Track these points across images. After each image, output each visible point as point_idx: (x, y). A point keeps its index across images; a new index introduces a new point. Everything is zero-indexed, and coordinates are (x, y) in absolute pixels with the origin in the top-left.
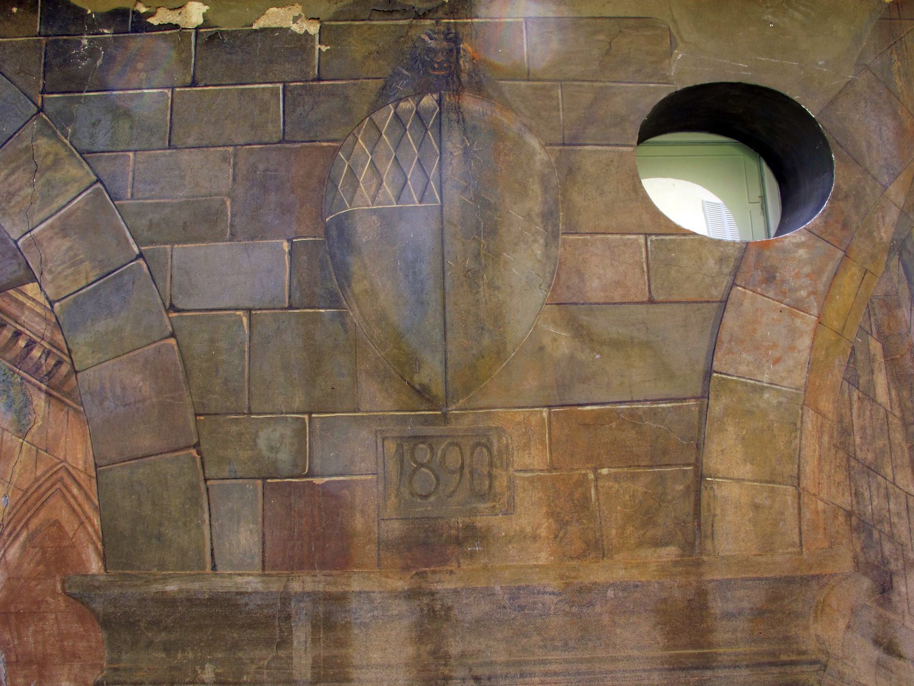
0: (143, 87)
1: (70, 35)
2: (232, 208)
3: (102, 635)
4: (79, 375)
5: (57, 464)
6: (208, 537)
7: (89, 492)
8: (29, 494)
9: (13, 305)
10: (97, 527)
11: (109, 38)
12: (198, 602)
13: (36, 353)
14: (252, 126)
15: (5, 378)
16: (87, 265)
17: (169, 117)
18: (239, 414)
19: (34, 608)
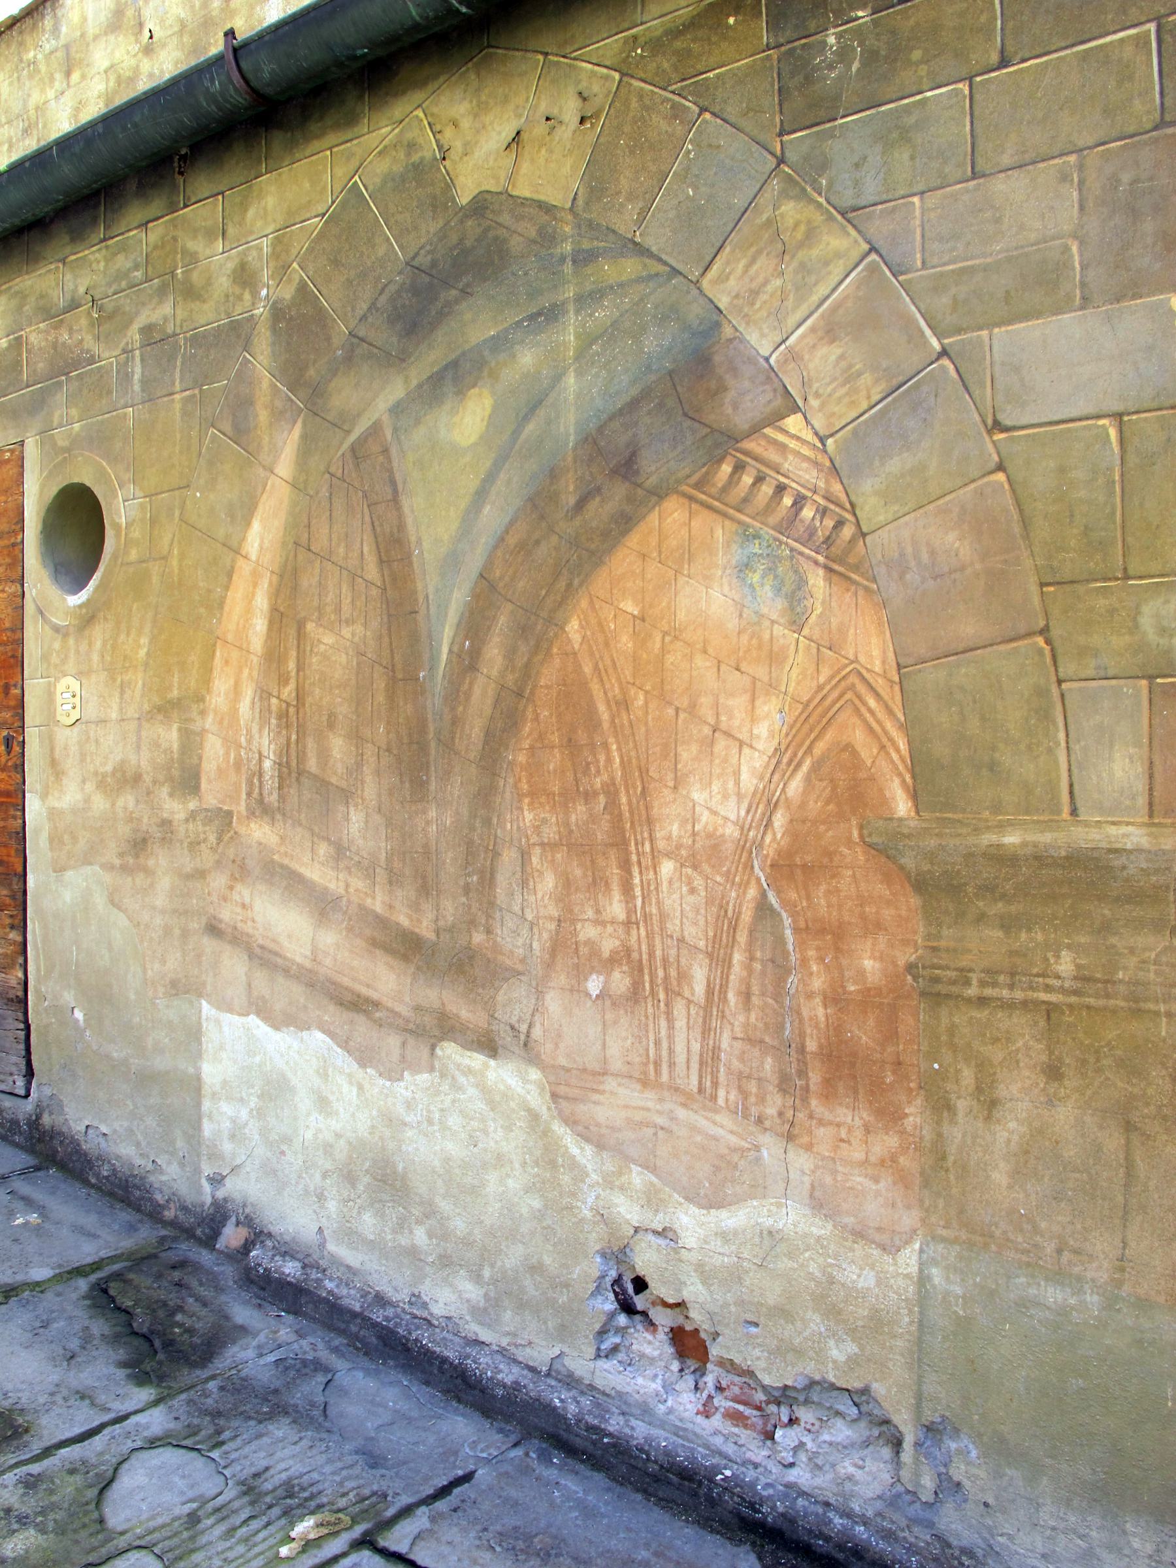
0: (925, 87)
1: (809, 36)
2: (1081, 255)
3: (915, 901)
4: (868, 539)
5: (846, 666)
6: (1064, 766)
7: (890, 703)
8: (811, 708)
9: (771, 449)
10: (903, 752)
11: (866, 23)
12: (1050, 861)
13: (808, 513)
14: (1106, 112)
15: (769, 551)
16: (867, 379)
17: (968, 128)
18: (1110, 579)
19: (825, 861)
